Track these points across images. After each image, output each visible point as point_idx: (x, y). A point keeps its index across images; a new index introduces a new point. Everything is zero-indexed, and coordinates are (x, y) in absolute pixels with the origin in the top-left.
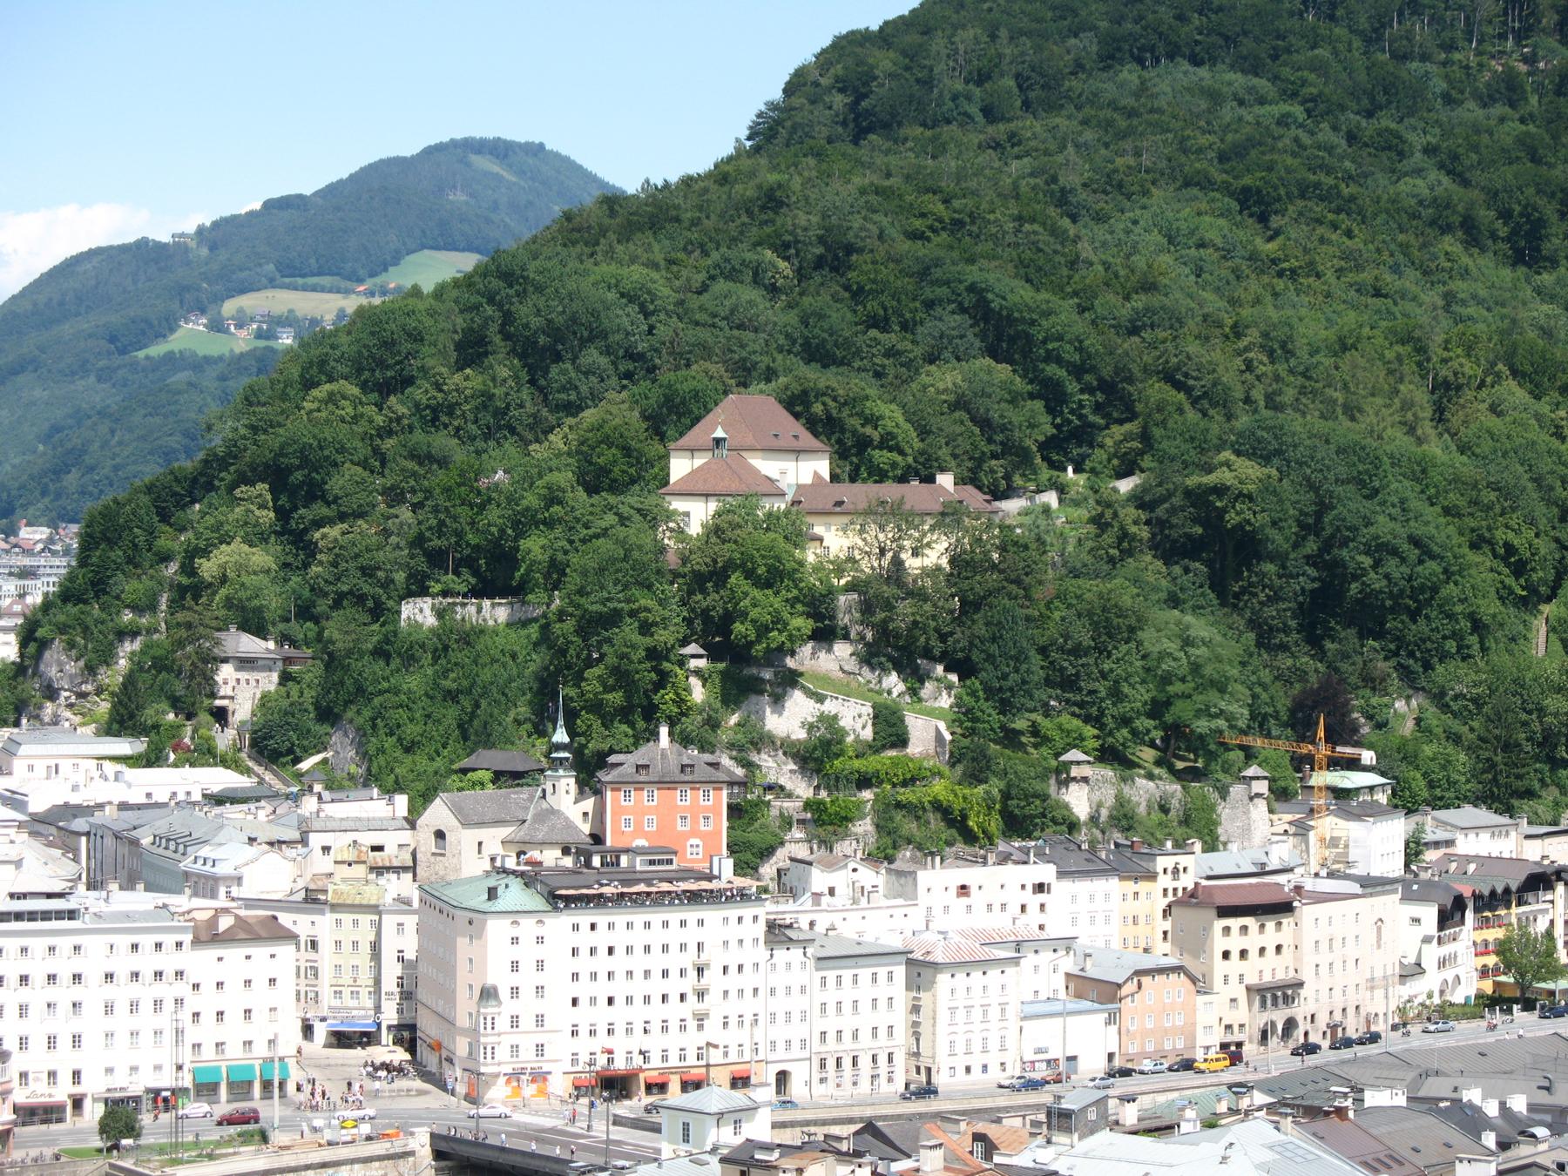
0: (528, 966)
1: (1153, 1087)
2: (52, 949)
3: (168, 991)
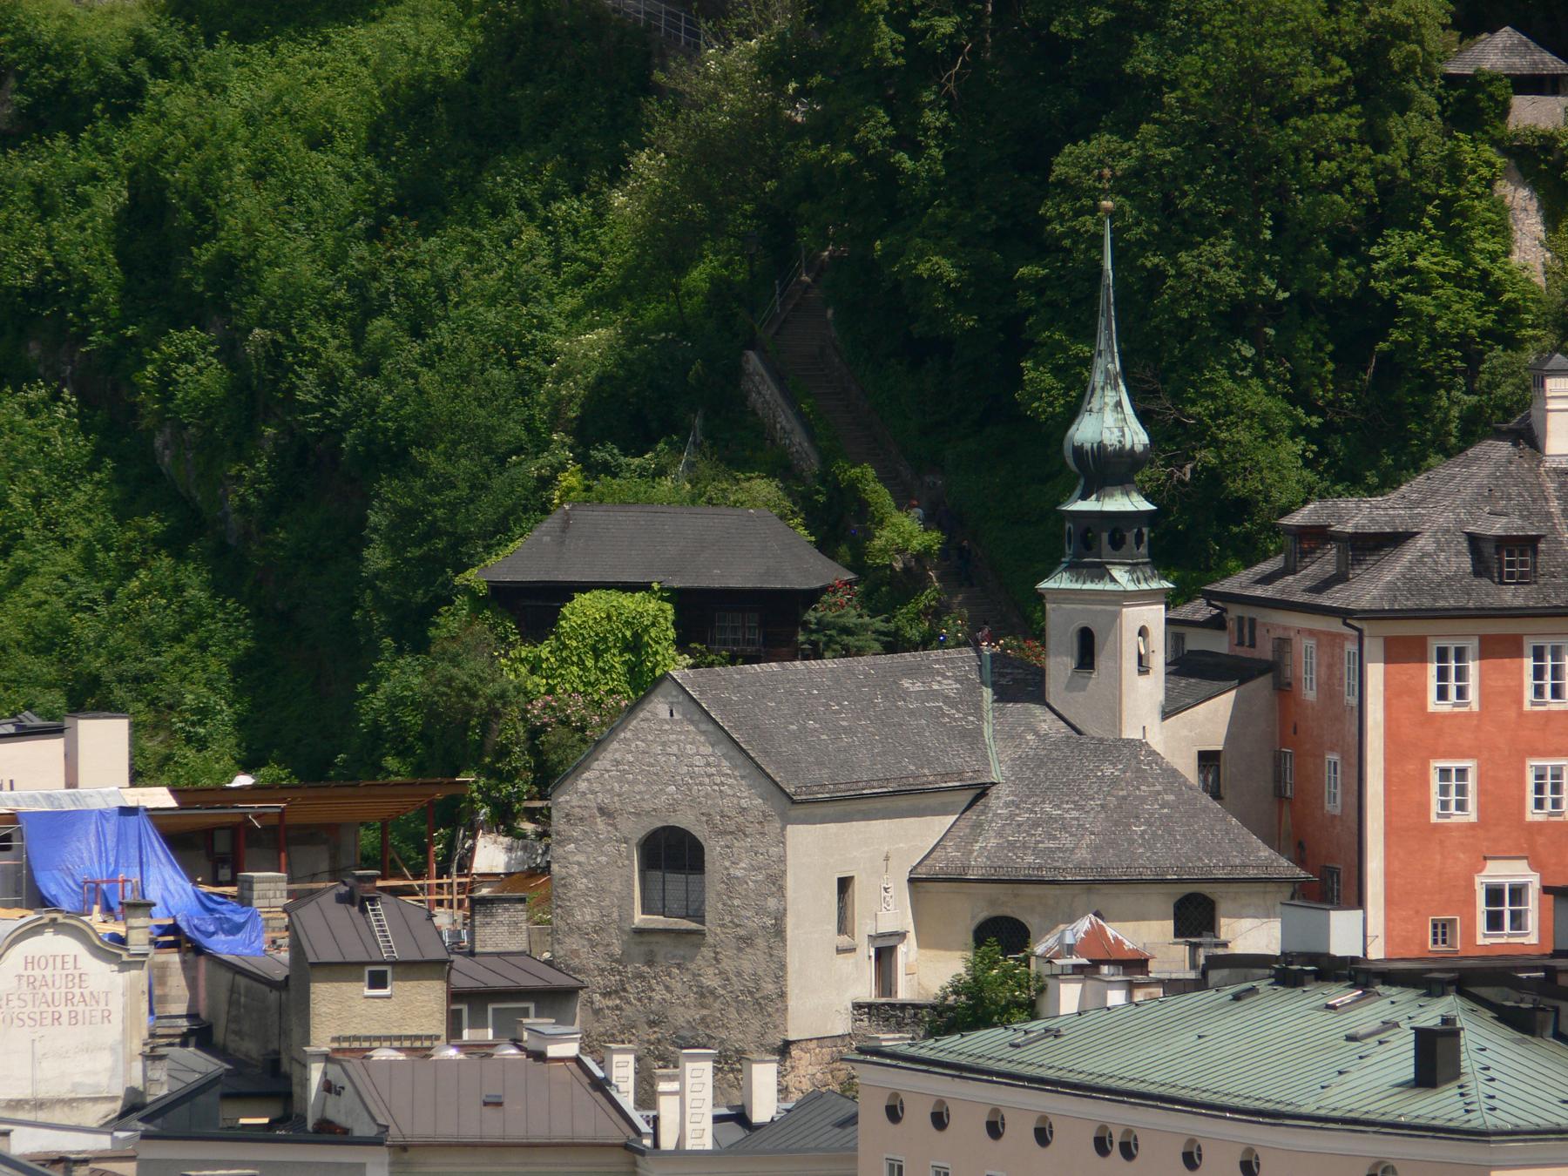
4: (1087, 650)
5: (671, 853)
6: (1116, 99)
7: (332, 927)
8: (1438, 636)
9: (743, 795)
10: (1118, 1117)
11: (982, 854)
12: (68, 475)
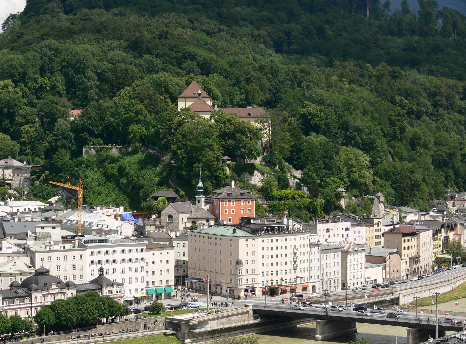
0: (250, 254)
1: (407, 287)
2: (92, 252)
3: (139, 265)
4: (199, 201)
5: (170, 217)
6: (198, 161)
7: (146, 222)
8: (248, 200)
9: (176, 212)
10: (210, 236)
11: (192, 216)
12: (115, 189)
